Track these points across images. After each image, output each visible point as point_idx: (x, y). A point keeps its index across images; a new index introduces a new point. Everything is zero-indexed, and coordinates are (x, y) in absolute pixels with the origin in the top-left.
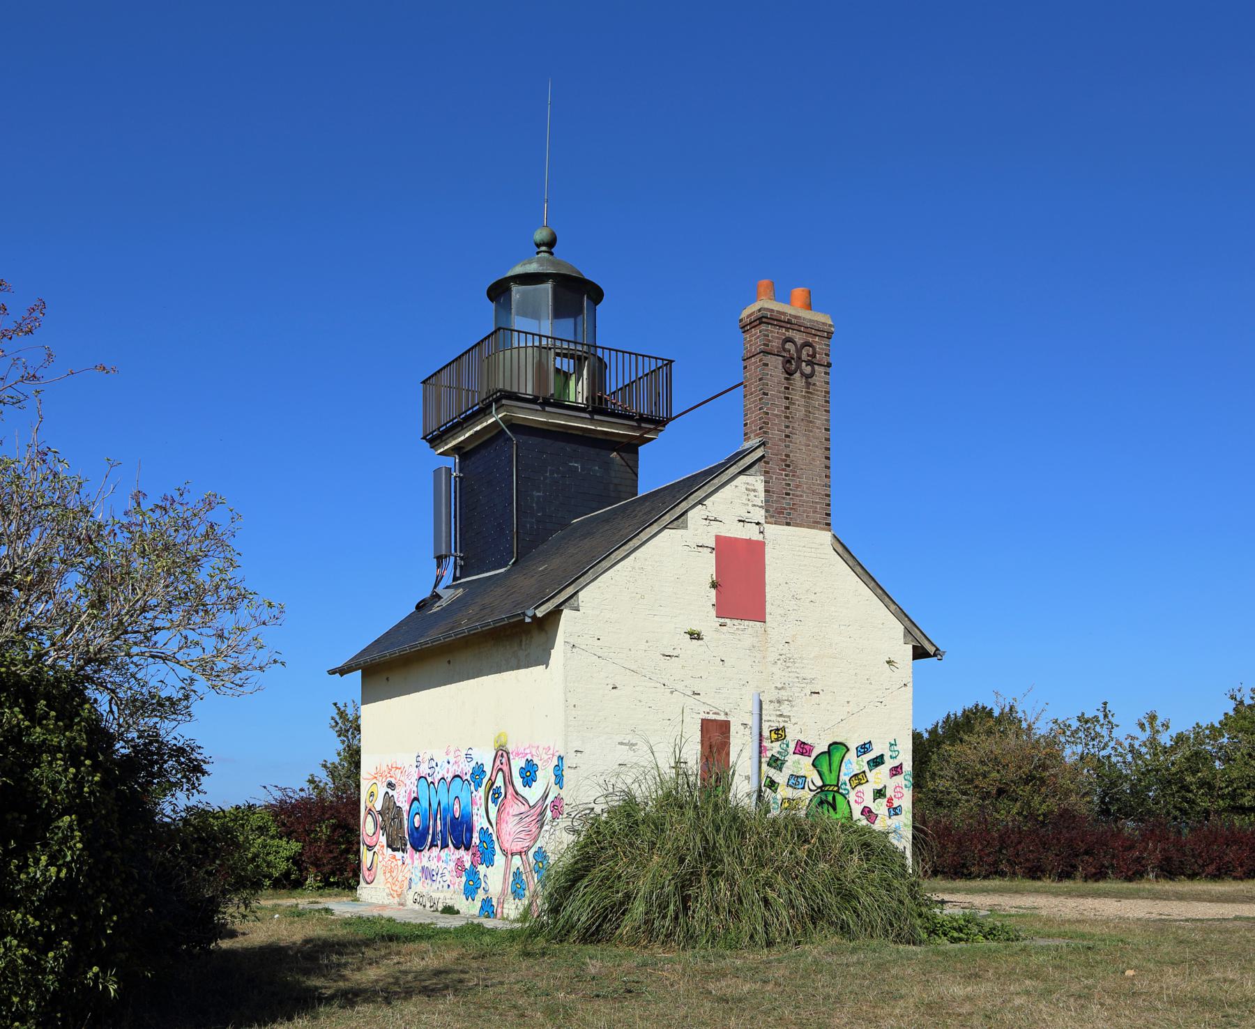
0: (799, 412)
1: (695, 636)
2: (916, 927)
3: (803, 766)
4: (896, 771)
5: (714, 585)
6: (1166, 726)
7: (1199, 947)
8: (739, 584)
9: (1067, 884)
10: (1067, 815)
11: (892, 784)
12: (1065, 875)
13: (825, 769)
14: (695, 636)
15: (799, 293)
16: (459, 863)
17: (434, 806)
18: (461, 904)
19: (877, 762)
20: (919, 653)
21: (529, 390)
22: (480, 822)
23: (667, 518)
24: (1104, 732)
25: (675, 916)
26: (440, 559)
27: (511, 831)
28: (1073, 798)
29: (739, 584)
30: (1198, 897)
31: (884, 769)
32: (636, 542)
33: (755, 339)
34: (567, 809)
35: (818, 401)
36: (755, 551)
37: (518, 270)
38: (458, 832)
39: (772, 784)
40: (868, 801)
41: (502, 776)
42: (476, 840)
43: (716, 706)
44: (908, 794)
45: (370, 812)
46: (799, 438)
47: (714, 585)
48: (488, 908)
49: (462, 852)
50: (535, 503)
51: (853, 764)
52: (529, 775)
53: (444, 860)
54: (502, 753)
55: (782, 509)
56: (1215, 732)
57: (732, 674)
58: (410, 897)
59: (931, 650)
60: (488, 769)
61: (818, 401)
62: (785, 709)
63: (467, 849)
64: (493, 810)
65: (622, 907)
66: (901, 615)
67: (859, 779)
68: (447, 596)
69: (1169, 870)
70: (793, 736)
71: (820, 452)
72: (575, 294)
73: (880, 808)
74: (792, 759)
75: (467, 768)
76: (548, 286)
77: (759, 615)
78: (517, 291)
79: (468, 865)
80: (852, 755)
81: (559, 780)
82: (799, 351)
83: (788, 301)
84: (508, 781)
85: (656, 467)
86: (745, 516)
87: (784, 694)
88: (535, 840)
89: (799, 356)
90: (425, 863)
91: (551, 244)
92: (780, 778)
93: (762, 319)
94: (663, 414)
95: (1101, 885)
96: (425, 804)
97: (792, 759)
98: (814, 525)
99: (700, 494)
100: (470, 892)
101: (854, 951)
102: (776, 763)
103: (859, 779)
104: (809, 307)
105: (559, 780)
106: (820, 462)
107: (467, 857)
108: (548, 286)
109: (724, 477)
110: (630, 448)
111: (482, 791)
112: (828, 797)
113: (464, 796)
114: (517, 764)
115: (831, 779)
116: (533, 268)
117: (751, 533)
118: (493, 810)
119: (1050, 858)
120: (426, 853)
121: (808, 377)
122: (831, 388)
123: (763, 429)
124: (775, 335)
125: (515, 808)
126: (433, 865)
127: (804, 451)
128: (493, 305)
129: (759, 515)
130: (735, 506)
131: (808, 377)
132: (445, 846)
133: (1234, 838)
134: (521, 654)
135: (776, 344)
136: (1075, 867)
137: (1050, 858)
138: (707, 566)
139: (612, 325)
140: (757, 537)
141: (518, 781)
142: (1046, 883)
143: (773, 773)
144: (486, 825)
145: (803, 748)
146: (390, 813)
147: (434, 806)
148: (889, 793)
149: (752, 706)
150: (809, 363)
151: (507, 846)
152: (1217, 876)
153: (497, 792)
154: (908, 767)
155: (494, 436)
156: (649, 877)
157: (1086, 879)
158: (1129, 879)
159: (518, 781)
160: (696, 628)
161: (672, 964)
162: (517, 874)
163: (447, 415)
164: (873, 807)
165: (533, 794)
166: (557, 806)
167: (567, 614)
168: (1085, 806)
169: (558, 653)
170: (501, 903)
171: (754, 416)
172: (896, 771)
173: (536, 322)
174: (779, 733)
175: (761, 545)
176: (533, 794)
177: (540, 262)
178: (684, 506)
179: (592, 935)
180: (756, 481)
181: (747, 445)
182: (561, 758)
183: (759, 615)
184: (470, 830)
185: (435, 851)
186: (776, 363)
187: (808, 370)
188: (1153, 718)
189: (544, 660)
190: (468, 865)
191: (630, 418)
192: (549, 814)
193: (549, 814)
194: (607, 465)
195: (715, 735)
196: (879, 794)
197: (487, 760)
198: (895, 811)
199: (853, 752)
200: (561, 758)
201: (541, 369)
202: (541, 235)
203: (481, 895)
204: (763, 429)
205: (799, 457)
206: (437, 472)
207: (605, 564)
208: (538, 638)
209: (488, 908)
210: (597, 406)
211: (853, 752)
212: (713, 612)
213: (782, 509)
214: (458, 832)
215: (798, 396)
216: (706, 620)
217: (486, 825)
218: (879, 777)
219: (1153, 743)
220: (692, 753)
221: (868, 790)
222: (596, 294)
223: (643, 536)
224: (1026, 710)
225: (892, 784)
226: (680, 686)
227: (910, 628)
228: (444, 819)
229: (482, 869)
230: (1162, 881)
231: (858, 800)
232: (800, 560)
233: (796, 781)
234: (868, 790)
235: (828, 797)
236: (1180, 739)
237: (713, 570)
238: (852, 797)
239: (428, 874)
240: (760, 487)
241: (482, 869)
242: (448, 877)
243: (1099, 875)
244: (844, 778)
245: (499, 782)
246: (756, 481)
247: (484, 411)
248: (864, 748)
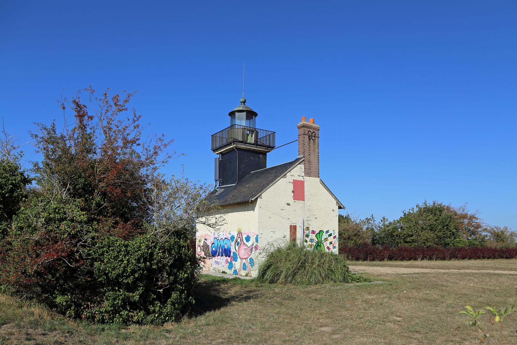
0: (312, 149)
1: (288, 204)
2: (347, 278)
3: (313, 236)
4: (335, 237)
5: (293, 192)
6: (387, 220)
7: (416, 283)
8: (298, 191)
9: (366, 262)
10: (365, 244)
11: (334, 241)
12: (365, 259)
13: (318, 237)
14: (288, 204)
15: (311, 119)
16: (227, 260)
17: (219, 245)
18: (227, 271)
19: (330, 235)
20: (340, 208)
21: (240, 139)
22: (233, 250)
23: (282, 175)
24: (372, 222)
25: (292, 277)
26: (216, 181)
27: (243, 253)
28: (367, 240)
29: (298, 191)
30: (401, 266)
31: (332, 237)
32: (275, 181)
33: (302, 131)
34: (259, 248)
35: (316, 146)
36: (302, 183)
37: (237, 109)
38: (227, 252)
39: (306, 241)
40: (328, 245)
41: (240, 239)
42: (232, 255)
43: (293, 222)
44: (337, 243)
45: (199, 246)
46: (312, 155)
47: (293, 192)
48: (235, 272)
49: (228, 257)
50: (244, 169)
51: (325, 236)
52: (248, 239)
53: (222, 260)
54: (240, 233)
55: (308, 173)
56: (398, 222)
57: (297, 214)
58: (212, 268)
59: (342, 207)
60: (236, 237)
61: (316, 146)
62: (309, 222)
63: (229, 257)
64: (237, 247)
65: (278, 275)
66: (336, 198)
67: (326, 239)
68: (220, 191)
69: (390, 258)
70: (311, 229)
71: (317, 159)
72: (251, 115)
73: (331, 247)
74: (311, 235)
75: (229, 236)
76: (245, 113)
77: (303, 199)
78: (237, 114)
79: (229, 261)
80: (324, 234)
81: (257, 241)
82: (312, 134)
83: (309, 122)
84: (242, 240)
85: (272, 160)
86: (300, 174)
87: (309, 219)
88: (250, 256)
89: (312, 135)
90: (216, 260)
91: (244, 102)
92: (308, 240)
93: (304, 126)
94: (272, 145)
95: (374, 262)
96: (216, 245)
97: (311, 235)
98: (315, 176)
99: (290, 169)
100: (230, 267)
101: (337, 286)
102: (307, 236)
103: (326, 239)
104: (314, 123)
105: (257, 241)
106: (317, 161)
107: (229, 259)
108: (245, 113)
109: (295, 165)
110: (264, 154)
111: (234, 242)
112: (319, 245)
113: (228, 243)
114: (244, 236)
115: (320, 240)
116: (241, 109)
117: (301, 179)
118: (237, 247)
119: (361, 255)
120: (216, 257)
121: (314, 140)
122: (319, 143)
123: (304, 153)
124: (307, 130)
125: (243, 247)
126: (219, 260)
127: (313, 158)
128: (230, 117)
129: (303, 174)
130: (297, 172)
131: (314, 140)
132: (222, 256)
133: (406, 250)
134: (246, 209)
135: (307, 132)
136: (367, 257)
137: (361, 255)
138: (291, 187)
139: (259, 123)
140: (302, 180)
141: (245, 241)
142: (360, 262)
143: (307, 238)
144: (235, 251)
145: (313, 232)
146: (205, 247)
147: (219, 245)
148: (333, 243)
149: (302, 222)
150: (314, 137)
151: (241, 257)
152: (402, 259)
153: (238, 243)
154: (337, 236)
155: (232, 150)
156: (285, 267)
157: (370, 260)
158: (381, 261)
159: (245, 241)
160: (289, 203)
161: (297, 290)
162: (244, 264)
163: (218, 145)
164: (329, 246)
165: (249, 244)
166: (256, 248)
167: (259, 199)
168: (369, 241)
169: (257, 208)
170: (240, 271)
171: (301, 150)
172: (335, 237)
173: (241, 121)
174: (308, 228)
175: (304, 182)
176: (249, 244)
177: (242, 107)
178: (286, 172)
179: (272, 282)
180: (302, 166)
181: (300, 157)
182: (257, 235)
183: (303, 199)
184: (230, 252)
185: (219, 257)
186: (307, 137)
187: (314, 138)
188: (384, 218)
189: (253, 209)
190: (229, 261)
191: (265, 146)
192: (254, 249)
193: (254, 249)
194: (259, 158)
195: (293, 229)
196: (331, 243)
197: (235, 235)
198: (334, 247)
199: (325, 233)
200: (257, 235)
201: (243, 133)
202: (242, 100)
203: (233, 269)
204: (304, 153)
205: (312, 160)
206: (216, 159)
207: (268, 187)
208: (251, 205)
209: (235, 272)
210: (256, 144)
211: (325, 233)
212: (293, 198)
213: (308, 173)
214: (227, 252)
215: (312, 145)
216: (291, 200)
217: (235, 251)
218: (331, 239)
219: (384, 225)
220: (288, 233)
221: (328, 242)
222: (256, 114)
223: (277, 180)
224: (353, 218)
225: (334, 241)
226: (285, 217)
227: (338, 202)
228: (222, 249)
229: (234, 262)
230: (389, 261)
231: (327, 244)
232: (312, 185)
233: (312, 240)
234: (328, 242)
235: (319, 245)
236: (390, 224)
237: (292, 188)
238: (324, 244)
239: (217, 263)
240: (303, 167)
241: (234, 262)
242: (223, 264)
243: (373, 260)
244: (323, 239)
245: (239, 240)
246: (302, 166)
247: (230, 144)
248: (327, 232)
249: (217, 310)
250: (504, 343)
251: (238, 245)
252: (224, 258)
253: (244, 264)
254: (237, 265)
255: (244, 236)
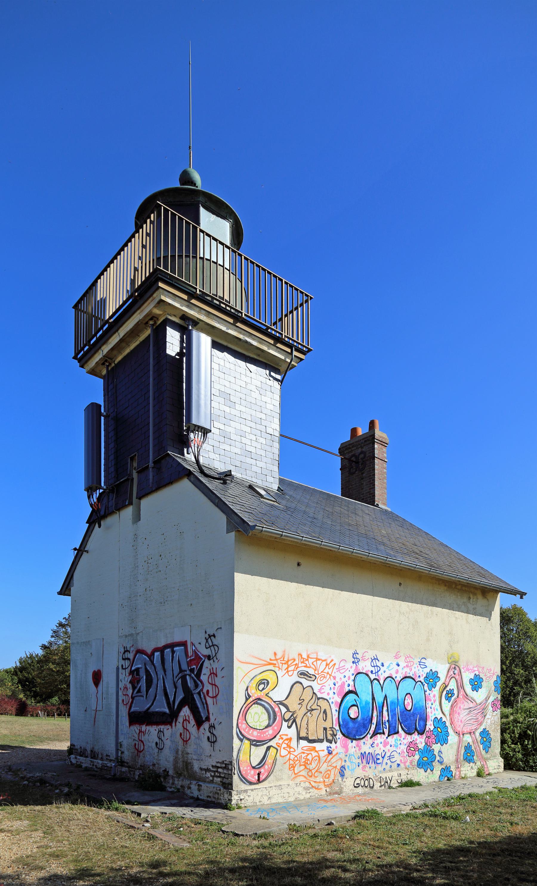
16: (412, 748)
17: (379, 699)
18: (419, 775)
38: (411, 721)
42: (430, 726)
49: (415, 736)
58: (348, 784)
60: (442, 675)
64: (447, 706)
75: (422, 673)
84: (460, 686)
88: (481, 724)
107: (420, 741)
111: (436, 691)
114: (467, 676)
120: (368, 740)
126: (378, 750)
132: (393, 732)
144: (439, 715)
147: (379, 699)
151: (459, 729)
159: (468, 688)
162: (468, 748)
184: (425, 719)
185: (380, 739)
190: (421, 746)
203: (438, 769)
208: (481, 602)
209: (447, 775)
214: (411, 721)
229: (436, 747)
241: (436, 747)
249: (96, 670)
250: (535, 763)
251: (448, 699)
252: (402, 740)
253: (468, 748)
254: (448, 752)
255: (467, 676)
